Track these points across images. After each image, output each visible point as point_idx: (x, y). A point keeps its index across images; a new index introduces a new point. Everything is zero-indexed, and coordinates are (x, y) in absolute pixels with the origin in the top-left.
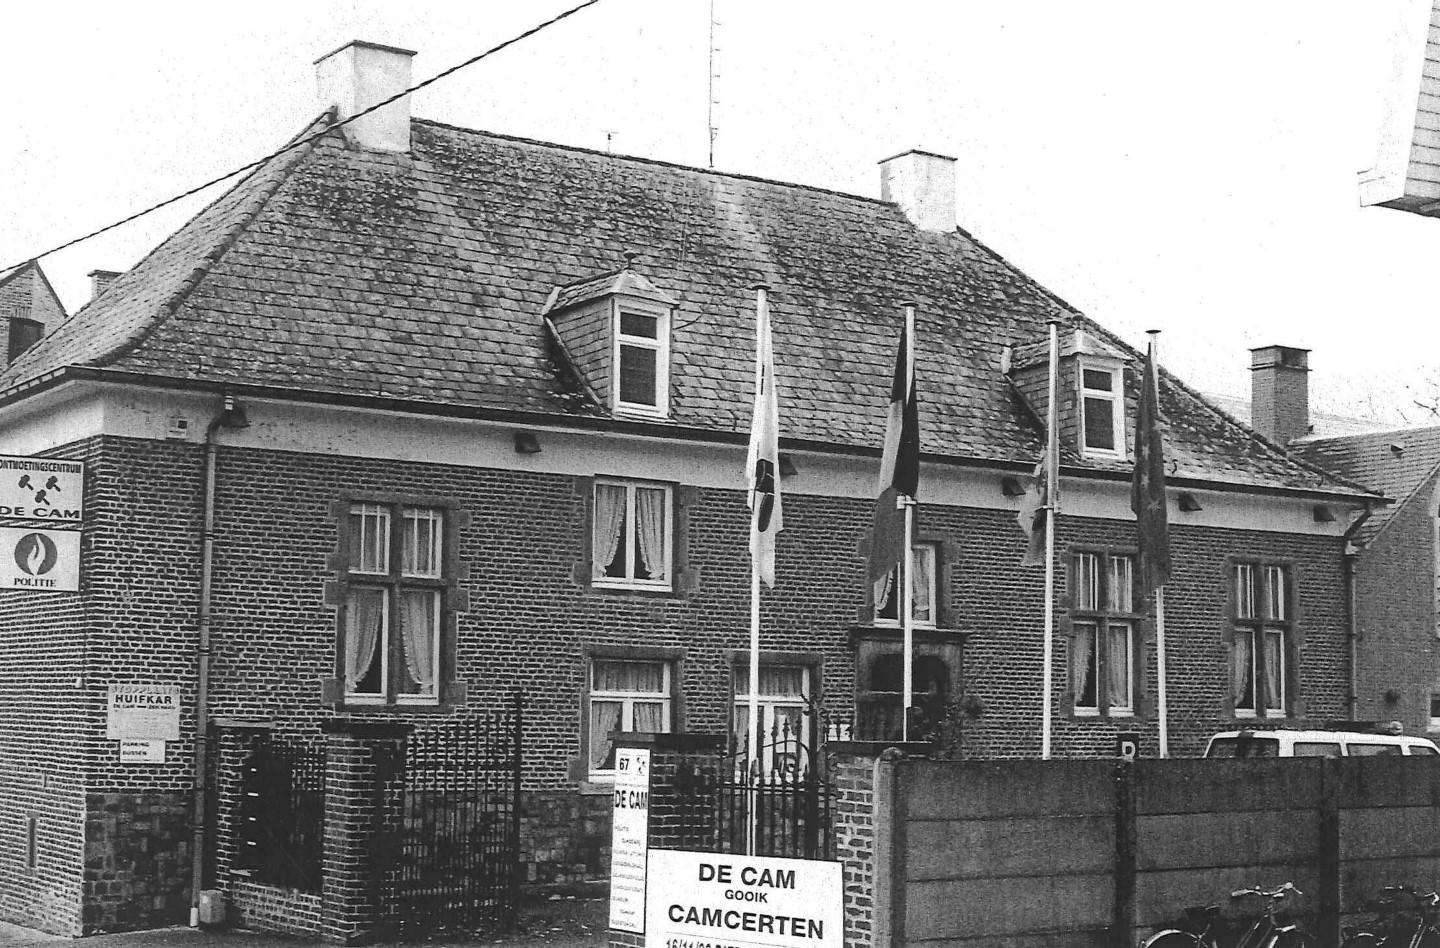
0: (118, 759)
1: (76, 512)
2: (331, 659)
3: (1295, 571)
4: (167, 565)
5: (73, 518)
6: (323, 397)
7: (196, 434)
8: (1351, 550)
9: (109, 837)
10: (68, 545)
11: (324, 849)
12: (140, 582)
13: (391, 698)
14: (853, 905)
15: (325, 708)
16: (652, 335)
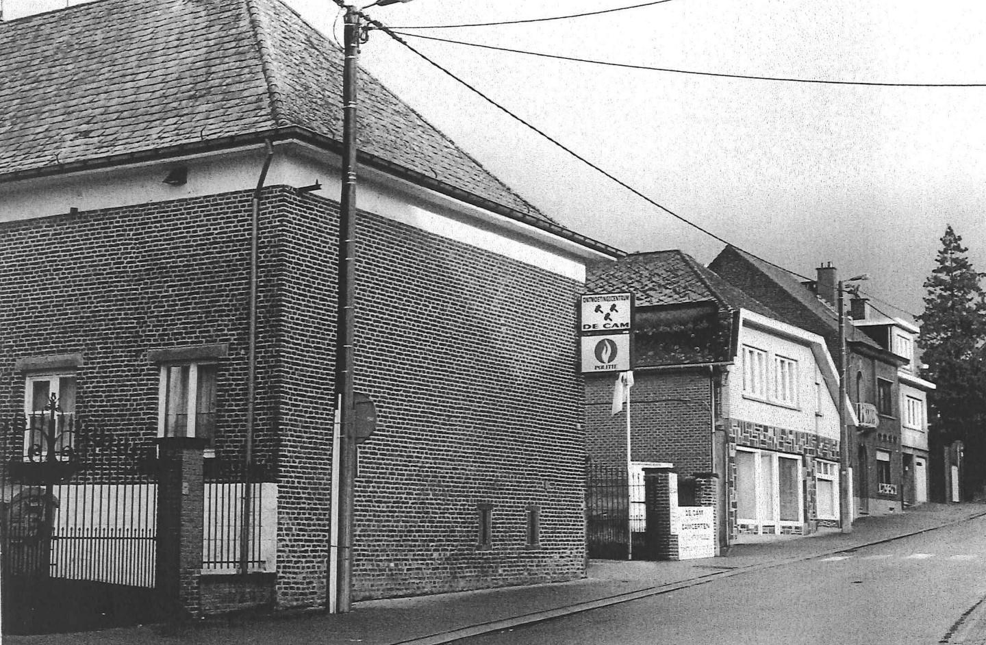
5: (626, 327)
11: (338, 298)
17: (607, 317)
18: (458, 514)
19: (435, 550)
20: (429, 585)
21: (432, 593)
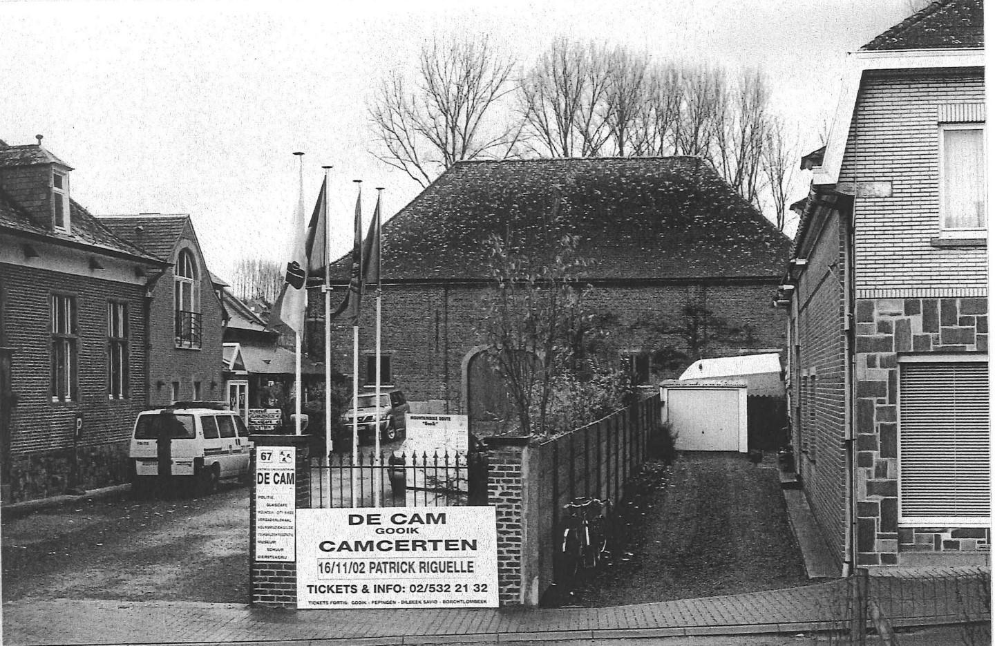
8: (149, 295)
14: (504, 529)
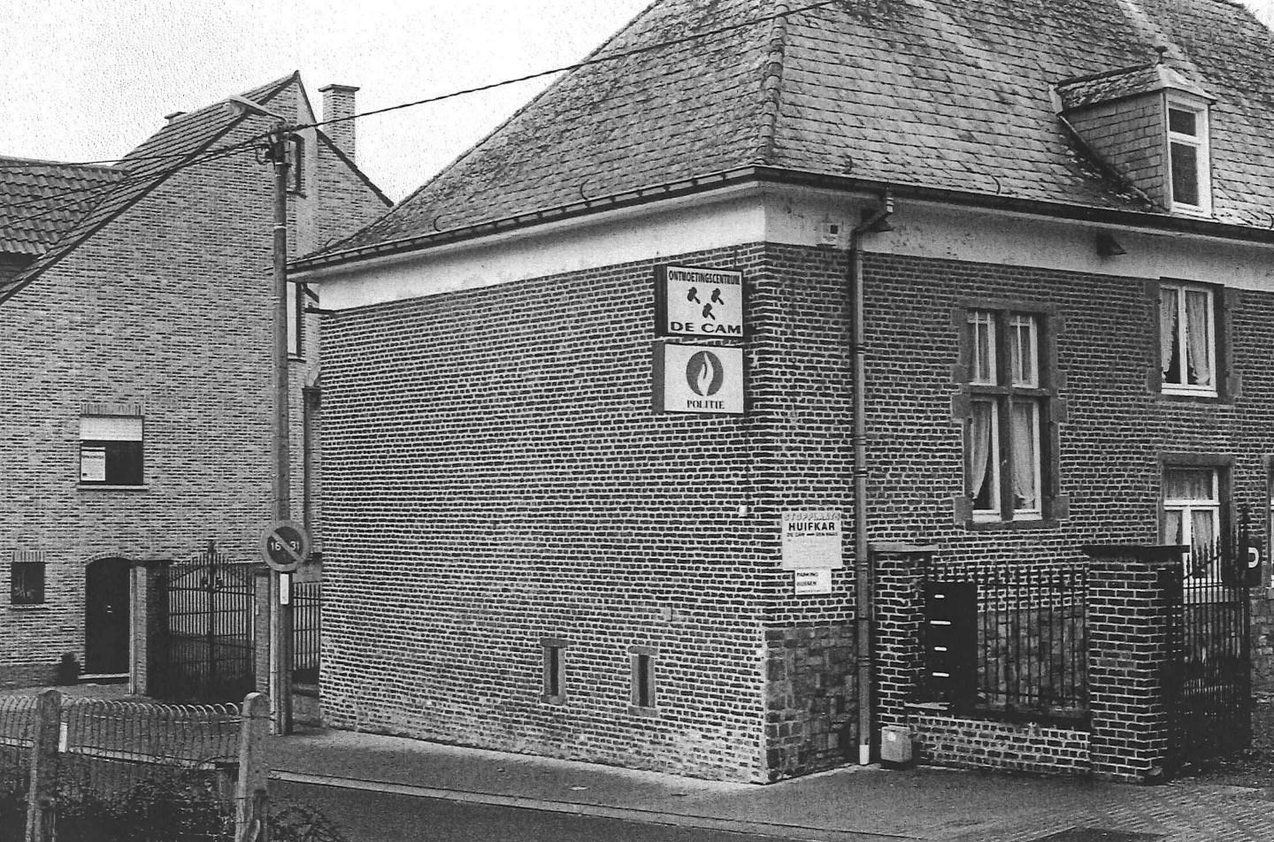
0: (793, 591)
1: (738, 327)
2: (960, 476)
3: (1051, 323)
4: (823, 382)
5: (735, 334)
6: (857, 184)
7: (841, 242)
9: (789, 674)
10: (732, 360)
12: (803, 401)
13: (1006, 513)
15: (957, 527)
16: (1191, 131)
17: (707, 311)
18: (512, 649)
19: (480, 694)
20: (475, 736)
21: (477, 747)
